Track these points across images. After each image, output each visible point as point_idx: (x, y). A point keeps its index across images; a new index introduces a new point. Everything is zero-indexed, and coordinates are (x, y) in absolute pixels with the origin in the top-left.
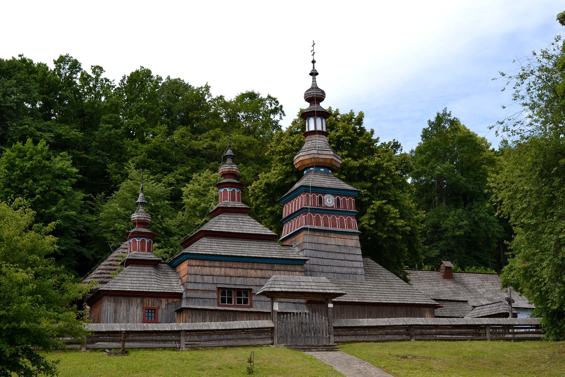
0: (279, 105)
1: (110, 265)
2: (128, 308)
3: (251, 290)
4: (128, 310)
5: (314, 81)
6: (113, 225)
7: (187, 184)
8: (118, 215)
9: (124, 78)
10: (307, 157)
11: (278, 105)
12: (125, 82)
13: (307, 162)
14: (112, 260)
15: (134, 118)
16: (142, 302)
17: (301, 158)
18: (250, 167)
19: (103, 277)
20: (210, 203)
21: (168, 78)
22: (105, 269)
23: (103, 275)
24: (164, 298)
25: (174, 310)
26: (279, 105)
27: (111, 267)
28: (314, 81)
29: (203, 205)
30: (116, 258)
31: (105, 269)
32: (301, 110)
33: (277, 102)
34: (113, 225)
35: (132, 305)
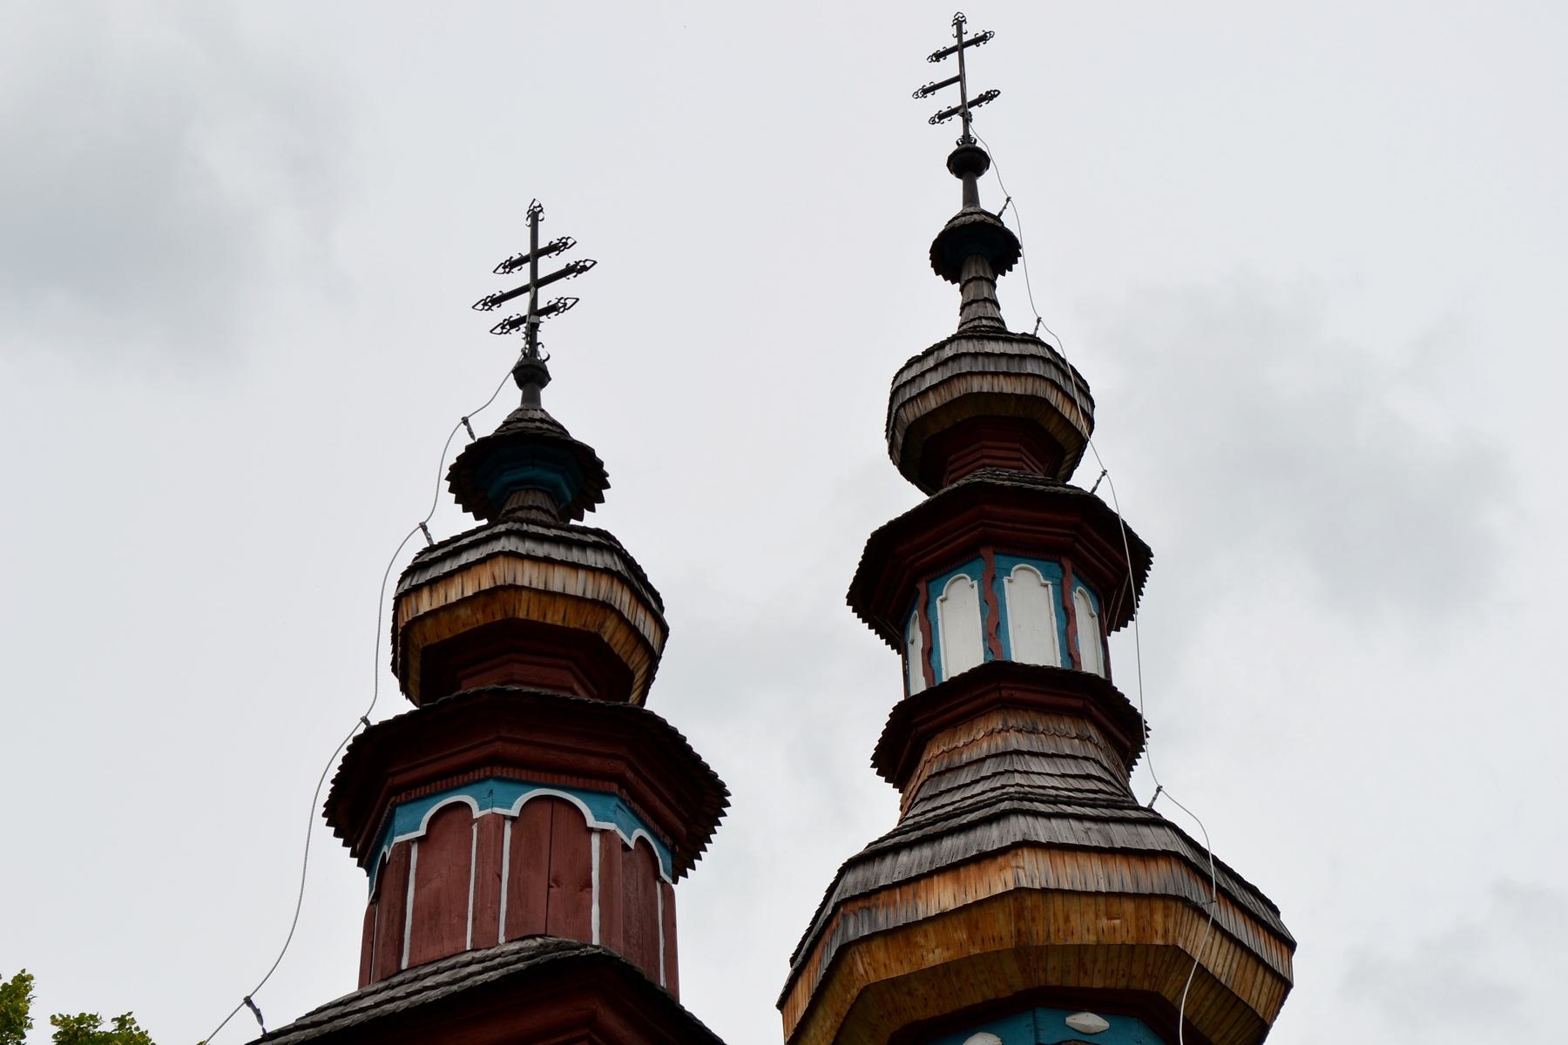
10: (1094, 876)
13: (1085, 928)
17: (1033, 871)
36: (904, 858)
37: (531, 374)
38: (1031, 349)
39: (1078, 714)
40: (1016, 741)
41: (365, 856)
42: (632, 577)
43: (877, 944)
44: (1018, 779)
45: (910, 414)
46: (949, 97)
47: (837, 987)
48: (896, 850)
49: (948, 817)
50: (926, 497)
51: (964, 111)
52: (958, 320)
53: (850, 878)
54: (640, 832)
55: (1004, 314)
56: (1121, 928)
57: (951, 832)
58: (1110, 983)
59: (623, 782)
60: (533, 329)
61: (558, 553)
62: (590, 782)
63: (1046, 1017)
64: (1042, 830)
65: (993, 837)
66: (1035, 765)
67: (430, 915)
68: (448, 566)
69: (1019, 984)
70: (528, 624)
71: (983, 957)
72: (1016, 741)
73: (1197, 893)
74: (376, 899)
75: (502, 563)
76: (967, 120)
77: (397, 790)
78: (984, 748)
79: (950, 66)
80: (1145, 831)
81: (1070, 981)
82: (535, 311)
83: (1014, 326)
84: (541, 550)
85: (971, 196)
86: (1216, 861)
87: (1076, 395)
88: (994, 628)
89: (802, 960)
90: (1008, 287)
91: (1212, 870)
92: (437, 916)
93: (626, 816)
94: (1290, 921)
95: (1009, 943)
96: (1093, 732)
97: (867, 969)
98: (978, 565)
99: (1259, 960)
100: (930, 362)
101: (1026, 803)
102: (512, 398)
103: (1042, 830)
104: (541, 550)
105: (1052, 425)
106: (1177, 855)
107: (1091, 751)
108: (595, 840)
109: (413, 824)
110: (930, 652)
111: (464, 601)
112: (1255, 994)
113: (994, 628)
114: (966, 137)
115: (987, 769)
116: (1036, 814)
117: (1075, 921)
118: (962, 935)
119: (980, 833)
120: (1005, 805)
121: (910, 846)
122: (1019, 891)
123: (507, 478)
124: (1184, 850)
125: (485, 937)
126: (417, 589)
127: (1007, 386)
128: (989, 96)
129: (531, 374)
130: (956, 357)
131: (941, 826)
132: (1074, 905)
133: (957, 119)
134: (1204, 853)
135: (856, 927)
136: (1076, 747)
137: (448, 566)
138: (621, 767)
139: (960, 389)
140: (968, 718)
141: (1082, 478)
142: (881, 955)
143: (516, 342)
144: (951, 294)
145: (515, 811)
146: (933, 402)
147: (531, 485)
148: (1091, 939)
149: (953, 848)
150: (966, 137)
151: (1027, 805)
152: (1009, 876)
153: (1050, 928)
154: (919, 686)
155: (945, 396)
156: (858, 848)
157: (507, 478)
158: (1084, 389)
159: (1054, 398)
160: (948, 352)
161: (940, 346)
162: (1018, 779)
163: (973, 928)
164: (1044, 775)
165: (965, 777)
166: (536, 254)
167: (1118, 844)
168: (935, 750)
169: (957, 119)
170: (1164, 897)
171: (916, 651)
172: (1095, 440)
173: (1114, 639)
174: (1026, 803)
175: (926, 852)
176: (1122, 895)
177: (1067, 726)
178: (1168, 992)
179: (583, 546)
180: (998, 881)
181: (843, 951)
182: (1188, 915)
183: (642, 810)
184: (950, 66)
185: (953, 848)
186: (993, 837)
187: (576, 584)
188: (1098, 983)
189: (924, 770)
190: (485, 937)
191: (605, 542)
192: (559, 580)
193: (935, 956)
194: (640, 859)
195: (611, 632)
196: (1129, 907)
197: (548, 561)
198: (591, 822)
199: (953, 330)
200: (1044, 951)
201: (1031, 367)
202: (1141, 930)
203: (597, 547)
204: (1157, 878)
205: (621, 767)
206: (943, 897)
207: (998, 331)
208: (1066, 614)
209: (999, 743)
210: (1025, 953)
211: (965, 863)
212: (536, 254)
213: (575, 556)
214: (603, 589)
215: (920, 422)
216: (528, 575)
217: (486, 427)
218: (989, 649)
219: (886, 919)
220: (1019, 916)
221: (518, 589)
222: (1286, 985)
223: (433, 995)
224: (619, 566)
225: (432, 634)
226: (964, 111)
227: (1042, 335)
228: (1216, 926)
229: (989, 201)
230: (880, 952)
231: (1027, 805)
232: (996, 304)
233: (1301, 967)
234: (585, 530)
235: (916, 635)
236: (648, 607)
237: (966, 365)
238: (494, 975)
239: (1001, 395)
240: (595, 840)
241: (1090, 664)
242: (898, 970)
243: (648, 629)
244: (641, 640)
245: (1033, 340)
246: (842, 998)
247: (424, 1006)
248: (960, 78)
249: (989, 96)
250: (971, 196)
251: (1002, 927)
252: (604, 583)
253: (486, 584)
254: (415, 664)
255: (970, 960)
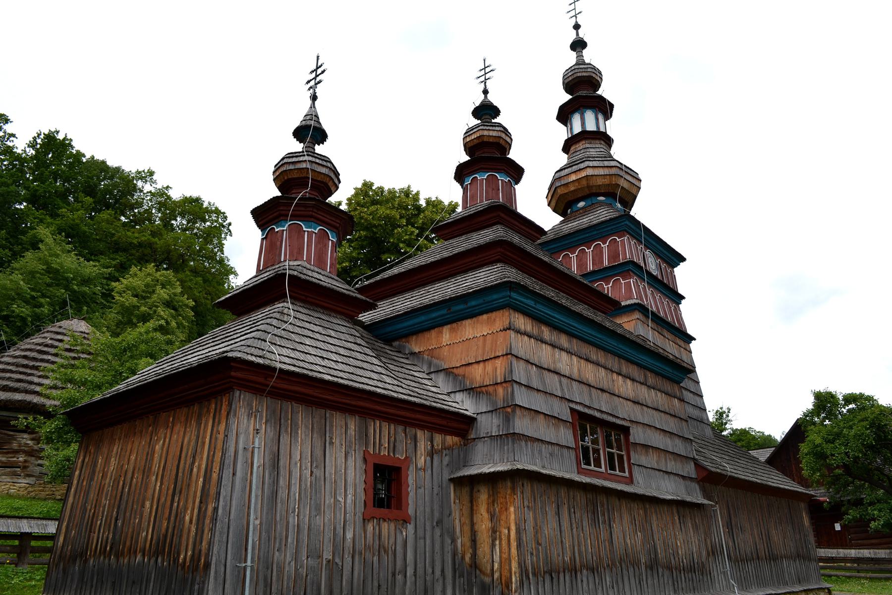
0: (227, 222)
1: (25, 357)
2: (318, 452)
3: (626, 431)
4: (319, 461)
5: (580, 56)
6: (7, 307)
7: (121, 279)
8: (18, 294)
9: (39, 135)
10: (601, 172)
11: (225, 222)
12: (39, 141)
13: (600, 182)
14: (30, 350)
15: (48, 183)
16: (364, 436)
17: (590, 172)
18: (200, 279)
19: (9, 379)
20: (154, 308)
21: (93, 157)
22: (13, 364)
23: (8, 375)
24: (422, 427)
25: (446, 476)
26: (227, 222)
27: (26, 362)
28: (580, 56)
29: (143, 309)
30: (39, 348)
31: (13, 364)
32: (367, 185)
33: (226, 218)
34: (7, 307)
35: (331, 443)
36: (566, 170)
37: (485, 92)
38: (589, 66)
39: (600, 139)
40: (588, 145)
41: (462, 185)
42: (505, 131)
43: (562, 187)
44: (588, 153)
45: (566, 81)
46: (573, 13)
47: (555, 194)
48: (565, 169)
49: (574, 162)
50: (570, 97)
51: (575, 16)
52: (576, 60)
53: (556, 174)
54: (509, 179)
55: (584, 58)
56: (606, 181)
57: (574, 165)
58: (605, 191)
59: (505, 170)
60: (485, 83)
61: (491, 128)
62: (499, 171)
63: (593, 198)
64: (591, 164)
65: (582, 166)
66: (591, 150)
67: (472, 197)
68: (471, 132)
69: (588, 193)
70: (486, 142)
71: (581, 188)
72: (588, 145)
73: (621, 173)
74: (464, 193)
75: (481, 131)
76: (576, 17)
77: (465, 175)
78: (581, 147)
79: (572, 7)
80: (611, 162)
81: (598, 191)
82: (486, 79)
83: (587, 61)
84: (488, 128)
85: (577, 34)
86: (625, 166)
87: (598, 74)
88: (583, 124)
89: (550, 189)
90: (585, 52)
91: (624, 168)
92: (473, 197)
93: (505, 176)
94: (641, 176)
95: (586, 185)
96: (602, 142)
97: (559, 191)
98: (579, 111)
99: (634, 184)
100: (570, 70)
101: (588, 159)
102: (483, 96)
103: (591, 164)
104: (488, 128)
105: (594, 81)
106: (617, 166)
107: (602, 146)
108: (500, 181)
109: (468, 181)
110: (571, 129)
111: (475, 139)
112: (634, 191)
113: (583, 124)
114: (576, 22)
115: (582, 152)
116: (590, 161)
117: (598, 180)
118: (577, 184)
119: (580, 165)
120: (584, 159)
121: (567, 168)
122: (587, 176)
123: (482, 113)
124: (619, 165)
125: (481, 201)
126: (466, 137)
127: (585, 74)
128: (580, 13)
129: (485, 92)
130: (574, 69)
131: (573, 164)
132: (598, 177)
133: (574, 17)
134: (621, 164)
135: (558, 184)
136: (599, 146)
137: (471, 132)
138: (504, 168)
139: (575, 76)
140: (578, 142)
141: (599, 92)
142: (562, 189)
143: (482, 86)
144: (574, 54)
145: (485, 177)
146: (570, 79)
147: (486, 114)
148: (601, 183)
149: (575, 168)
150: (576, 22)
151: (588, 159)
152: (585, 173)
153: (593, 182)
154: (570, 136)
155: (573, 77)
156: (558, 169)
157: (482, 113)
158: (600, 73)
159: (594, 75)
160: (573, 68)
161: (571, 67)
162: (588, 153)
163: (579, 183)
164: (593, 152)
165: (578, 153)
166: (485, 68)
167: (25, 521)
168: (572, 148)
169: (574, 17)
170: (615, 175)
171: (569, 128)
172: (603, 85)
173: (606, 122)
174: (588, 159)
175: (570, 169)
176: (607, 175)
177: (597, 142)
178: (616, 192)
179: (495, 126)
180: (583, 174)
181: (556, 188)
182: (619, 177)
183: (509, 175)
184: (572, 7)
185: (575, 168)
186: (582, 166)
187: (494, 134)
188: (603, 191)
189: (571, 152)
190: (481, 201)
191: (500, 125)
192: (491, 133)
193: (572, 189)
194: (508, 184)
195: (501, 141)
196: (608, 177)
197: (489, 130)
198: (499, 178)
199: (574, 63)
200: (592, 187)
201: (589, 70)
202: (610, 181)
203: (498, 126)
204: (613, 171)
205: (504, 168)
206: (573, 177)
207: (584, 63)
208: (597, 119)
209: (584, 146)
210: (589, 187)
211: (577, 171)
212: (485, 68)
213: (494, 128)
214: (499, 134)
215: (568, 82)
216: (486, 133)
217: (477, 104)
218: (582, 128)
219: (563, 182)
220: (587, 180)
221: (484, 136)
222: (640, 188)
223: (472, 212)
224: (502, 129)
225: (470, 145)
226: (575, 16)
227: (591, 63)
228: (625, 179)
229: (581, 35)
230: (562, 188)
231: (588, 159)
232: (583, 56)
233: (643, 185)
234: (496, 123)
235: (569, 125)
236: (508, 136)
237: (576, 71)
238: (482, 209)
239: (584, 76)
240: (500, 181)
241: (602, 129)
242: (566, 192)
243: (509, 140)
244: (508, 142)
245: (590, 64)
246: (556, 197)
247: (471, 214)
248: (575, 9)
249: (580, 13)
250: (577, 34)
251: (584, 182)
252: (500, 133)
253: (478, 135)
254: (467, 150)
255: (579, 189)
